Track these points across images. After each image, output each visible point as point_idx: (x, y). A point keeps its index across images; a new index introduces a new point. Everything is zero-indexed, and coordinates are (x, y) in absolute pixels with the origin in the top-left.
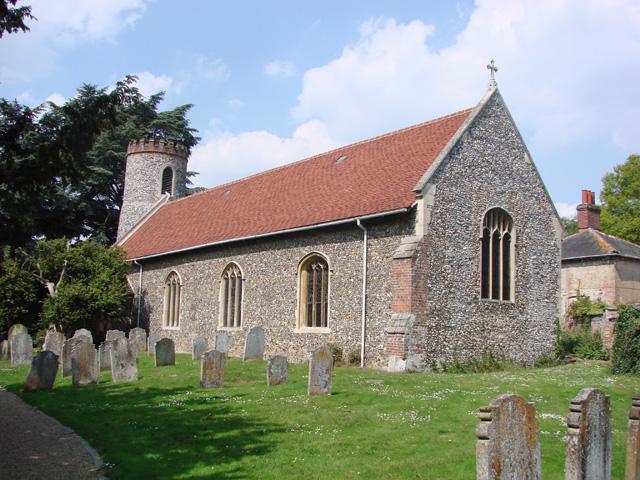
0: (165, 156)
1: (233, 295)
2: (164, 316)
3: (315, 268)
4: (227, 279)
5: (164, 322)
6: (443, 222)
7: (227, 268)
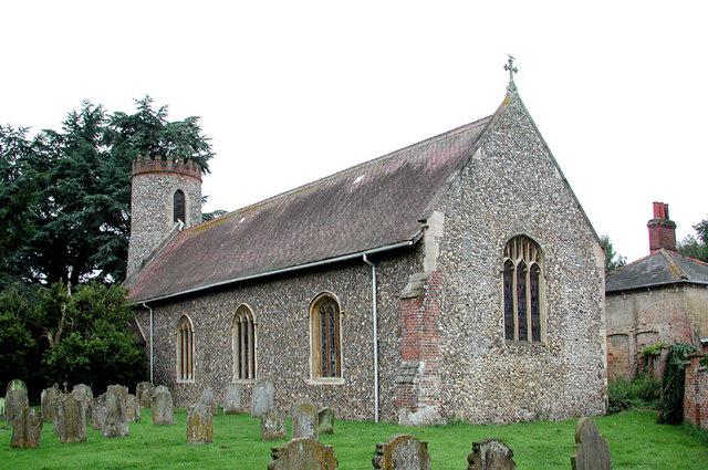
0: (175, 176)
1: (246, 342)
2: (178, 367)
3: (326, 306)
4: (239, 324)
5: (178, 374)
6: (454, 254)
7: (238, 312)
